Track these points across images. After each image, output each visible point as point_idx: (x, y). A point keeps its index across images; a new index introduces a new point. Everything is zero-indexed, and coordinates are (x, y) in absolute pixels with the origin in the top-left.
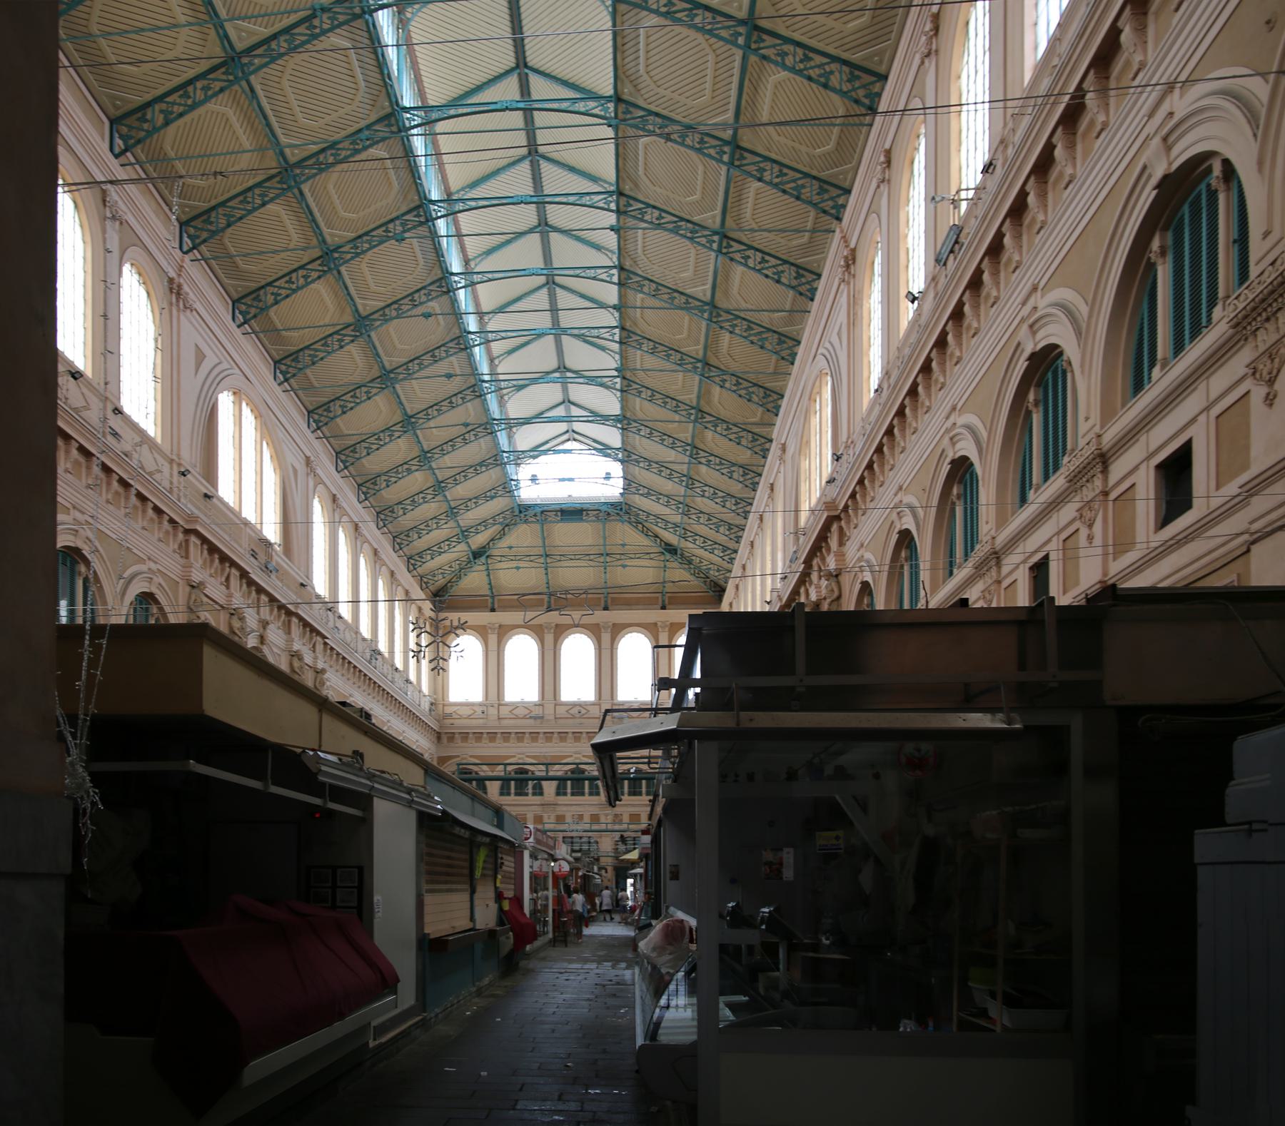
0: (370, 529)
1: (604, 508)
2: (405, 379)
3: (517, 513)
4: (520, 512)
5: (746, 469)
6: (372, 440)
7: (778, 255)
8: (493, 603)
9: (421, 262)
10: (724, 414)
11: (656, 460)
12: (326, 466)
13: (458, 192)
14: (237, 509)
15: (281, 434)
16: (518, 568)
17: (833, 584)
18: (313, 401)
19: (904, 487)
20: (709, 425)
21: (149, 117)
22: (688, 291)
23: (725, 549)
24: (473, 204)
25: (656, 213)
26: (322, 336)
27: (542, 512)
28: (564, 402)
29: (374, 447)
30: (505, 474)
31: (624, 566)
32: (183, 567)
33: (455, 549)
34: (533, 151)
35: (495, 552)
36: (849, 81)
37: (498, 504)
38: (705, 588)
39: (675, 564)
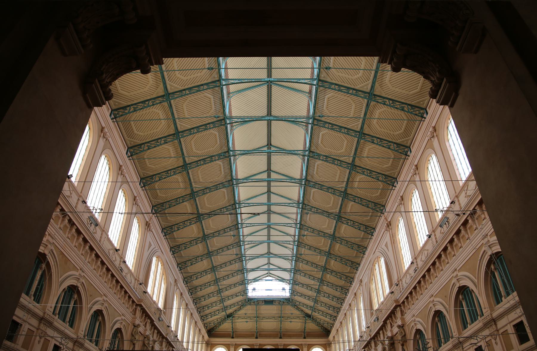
0: (192, 306)
1: (282, 300)
2: (216, 255)
3: (247, 301)
4: (248, 301)
5: (342, 288)
6: (199, 274)
7: (359, 222)
8: (233, 335)
9: (227, 198)
10: (334, 269)
11: (306, 284)
12: (181, 283)
13: (243, 201)
14: (151, 296)
15: (169, 271)
16: (247, 322)
17: (402, 330)
18: (179, 260)
19: (434, 295)
20: (329, 273)
22: (324, 231)
23: (331, 316)
24: (252, 204)
25: (316, 209)
26: (190, 240)
27: (257, 301)
28: (268, 263)
29: (199, 277)
30: (246, 287)
31: (291, 322)
32: (132, 318)
33: (220, 314)
34: (269, 191)
35: (236, 316)
37: (240, 298)
38: (322, 331)
39: (310, 321)
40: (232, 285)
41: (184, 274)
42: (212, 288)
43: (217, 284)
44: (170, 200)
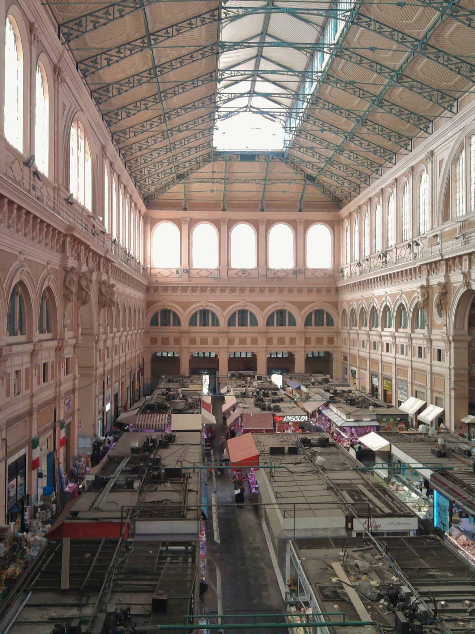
18: (80, 55)
21: (99, 61)
36: (470, 72)
40: (192, 148)
41: (75, 52)
42: (144, 90)
43: (155, 80)
44: (93, 11)
